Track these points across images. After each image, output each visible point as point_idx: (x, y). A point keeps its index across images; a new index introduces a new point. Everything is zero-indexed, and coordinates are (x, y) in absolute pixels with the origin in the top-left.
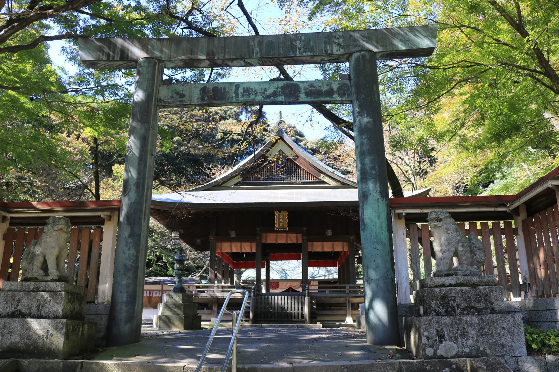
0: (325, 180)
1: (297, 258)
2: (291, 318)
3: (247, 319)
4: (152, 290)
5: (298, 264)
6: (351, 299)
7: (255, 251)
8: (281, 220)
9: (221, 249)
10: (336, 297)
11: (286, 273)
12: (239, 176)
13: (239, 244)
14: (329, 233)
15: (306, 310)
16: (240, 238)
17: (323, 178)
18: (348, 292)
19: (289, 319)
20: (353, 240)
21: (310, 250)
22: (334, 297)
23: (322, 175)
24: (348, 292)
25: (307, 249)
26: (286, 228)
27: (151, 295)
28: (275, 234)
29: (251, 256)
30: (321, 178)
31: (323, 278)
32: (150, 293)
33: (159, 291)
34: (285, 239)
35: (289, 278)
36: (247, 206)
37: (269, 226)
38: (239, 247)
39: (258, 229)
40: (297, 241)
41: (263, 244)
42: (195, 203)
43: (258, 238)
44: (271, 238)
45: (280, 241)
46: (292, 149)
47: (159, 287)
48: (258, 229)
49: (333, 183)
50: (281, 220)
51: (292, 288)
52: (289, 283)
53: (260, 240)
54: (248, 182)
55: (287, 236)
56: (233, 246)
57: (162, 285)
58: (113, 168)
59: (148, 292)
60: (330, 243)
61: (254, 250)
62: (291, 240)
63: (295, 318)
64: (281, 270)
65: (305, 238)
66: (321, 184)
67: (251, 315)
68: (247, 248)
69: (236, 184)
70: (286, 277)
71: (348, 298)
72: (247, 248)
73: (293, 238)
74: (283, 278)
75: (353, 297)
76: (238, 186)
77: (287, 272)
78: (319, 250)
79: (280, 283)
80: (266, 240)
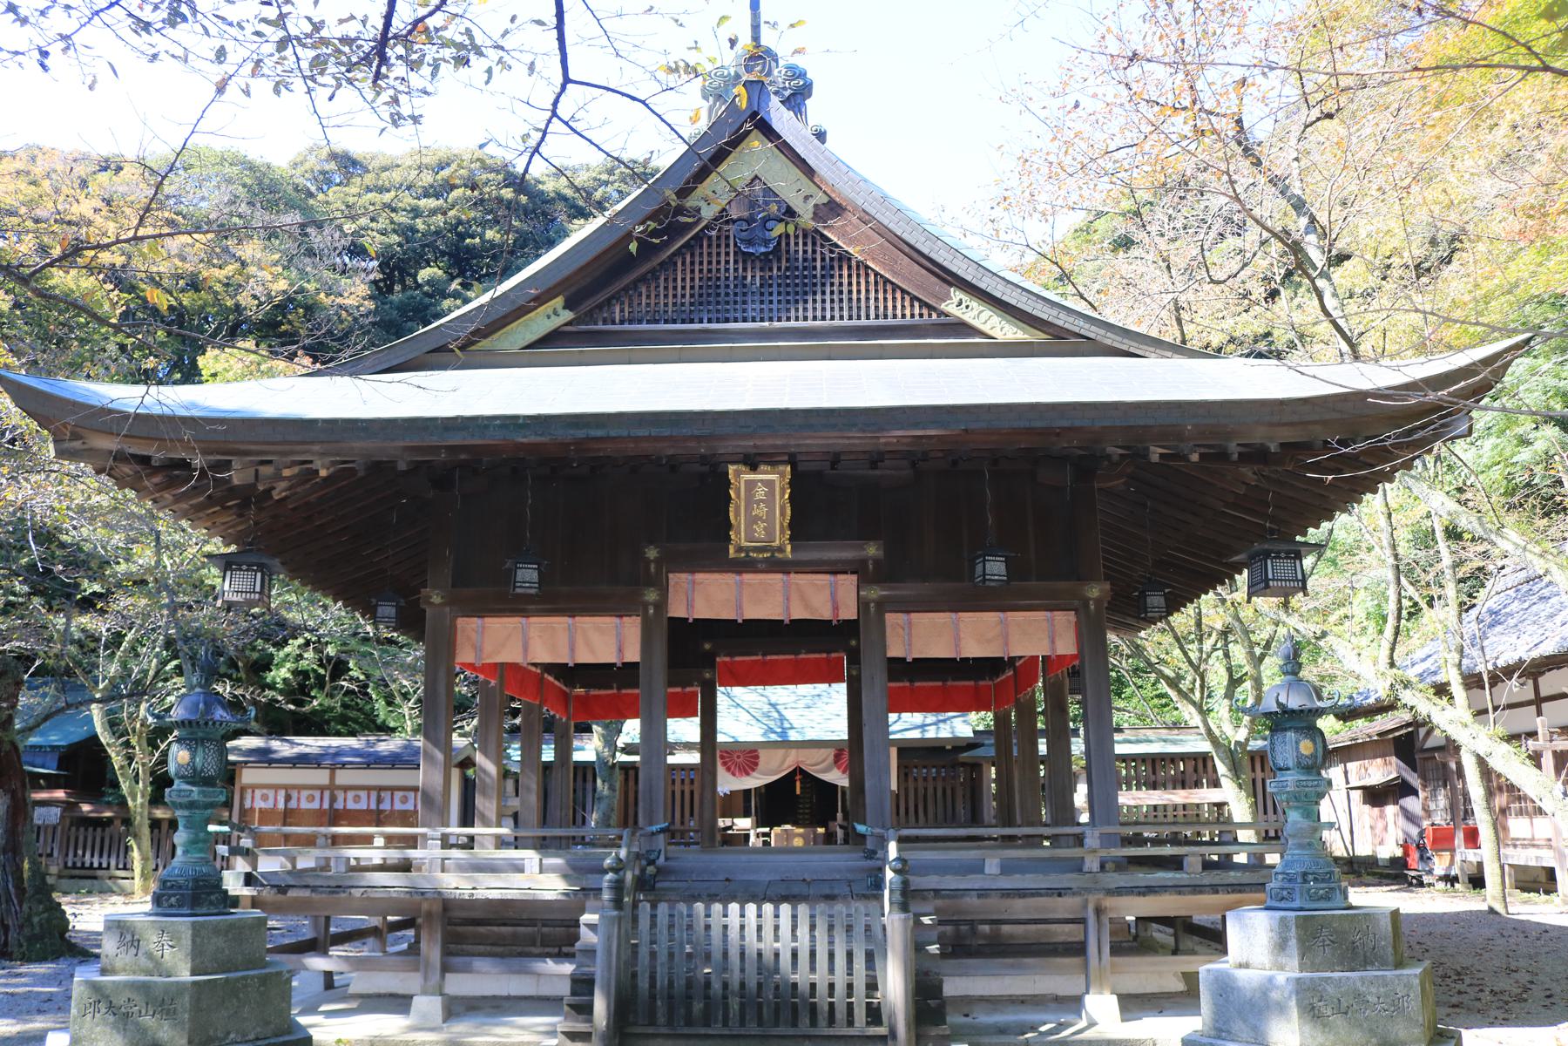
0: (968, 317)
1: (830, 677)
2: (814, 1023)
3: (581, 1027)
4: (294, 787)
5: (836, 696)
6: (1109, 902)
7: (637, 659)
8: (760, 502)
9: (478, 649)
10: (1035, 893)
11: (782, 718)
12: (558, 302)
13: (560, 622)
14: (996, 568)
15: (894, 985)
16: (559, 598)
17: (957, 305)
18: (1092, 863)
19: (804, 1027)
20: (1098, 601)
21: (894, 652)
22: (1022, 893)
23: (957, 295)
24: (1092, 863)
25: (884, 648)
26: (781, 549)
27: (293, 804)
28: (731, 578)
29: (626, 674)
30: (950, 307)
31: (916, 734)
32: (288, 798)
33: (322, 788)
34: (780, 598)
35: (793, 736)
36: (581, 434)
37: (701, 528)
38: (563, 640)
39: (652, 553)
40: (836, 608)
41: (677, 625)
42: (312, 422)
43: (651, 596)
44: (706, 596)
45: (754, 612)
46: (809, 171)
47: (320, 777)
48: (652, 553)
49: (1005, 330)
50: (760, 502)
51: (802, 772)
52: (793, 752)
53: (662, 605)
54: (600, 327)
55: (787, 586)
56: (534, 633)
57: (333, 769)
58: (201, 361)
59: (282, 793)
60: (991, 617)
61: (633, 655)
62: (807, 606)
63: (831, 1020)
64: (766, 708)
65: (874, 593)
66: (956, 339)
67: (600, 1006)
68: (606, 639)
69: (551, 339)
70: (784, 732)
71: (1092, 899)
72: (606, 639)
73: (823, 596)
74: (774, 737)
75: (1119, 891)
76: (553, 347)
77: (784, 712)
78: (939, 649)
79: (762, 754)
80: (690, 605)
